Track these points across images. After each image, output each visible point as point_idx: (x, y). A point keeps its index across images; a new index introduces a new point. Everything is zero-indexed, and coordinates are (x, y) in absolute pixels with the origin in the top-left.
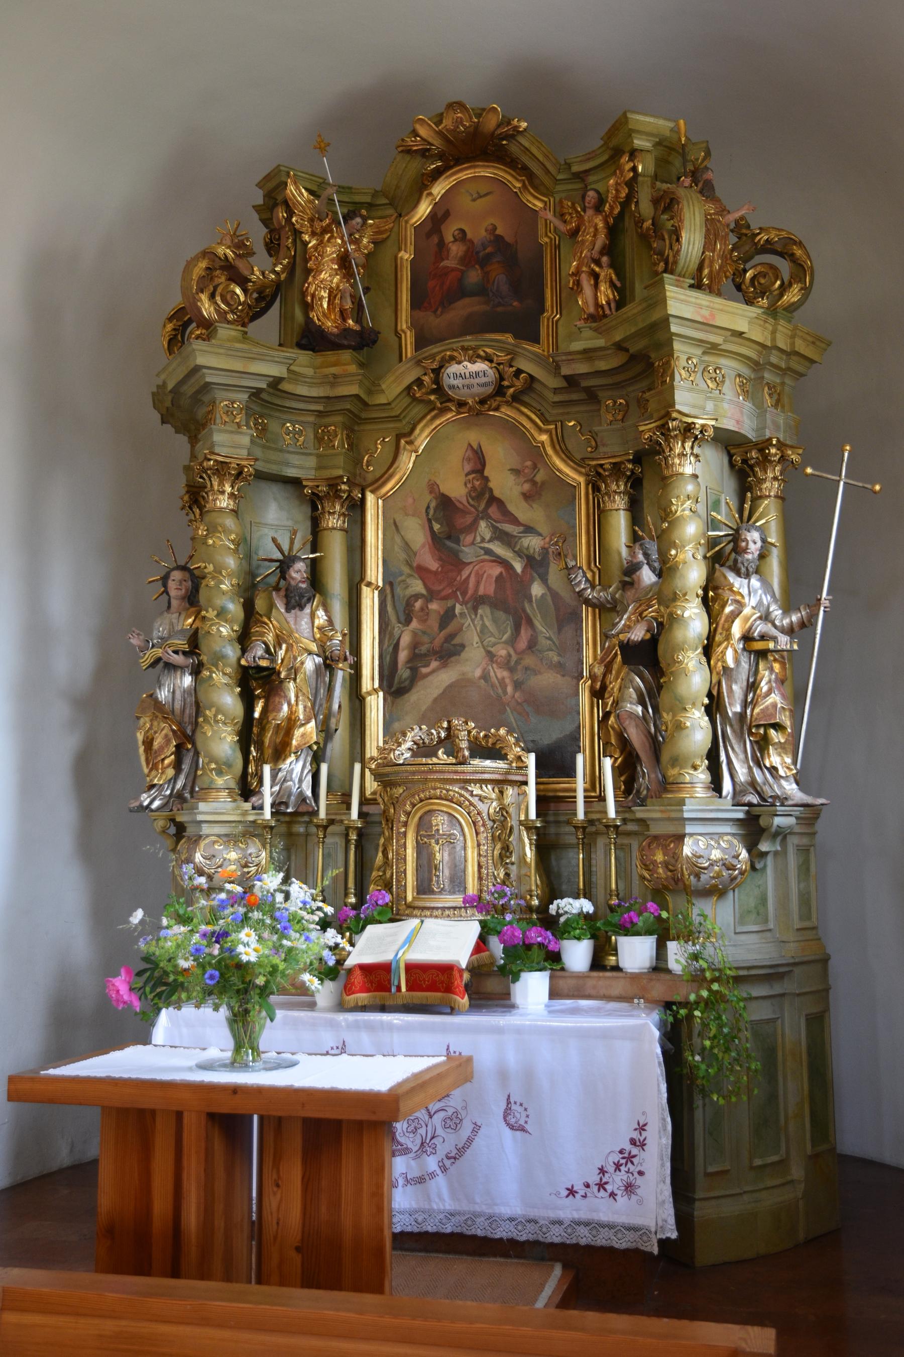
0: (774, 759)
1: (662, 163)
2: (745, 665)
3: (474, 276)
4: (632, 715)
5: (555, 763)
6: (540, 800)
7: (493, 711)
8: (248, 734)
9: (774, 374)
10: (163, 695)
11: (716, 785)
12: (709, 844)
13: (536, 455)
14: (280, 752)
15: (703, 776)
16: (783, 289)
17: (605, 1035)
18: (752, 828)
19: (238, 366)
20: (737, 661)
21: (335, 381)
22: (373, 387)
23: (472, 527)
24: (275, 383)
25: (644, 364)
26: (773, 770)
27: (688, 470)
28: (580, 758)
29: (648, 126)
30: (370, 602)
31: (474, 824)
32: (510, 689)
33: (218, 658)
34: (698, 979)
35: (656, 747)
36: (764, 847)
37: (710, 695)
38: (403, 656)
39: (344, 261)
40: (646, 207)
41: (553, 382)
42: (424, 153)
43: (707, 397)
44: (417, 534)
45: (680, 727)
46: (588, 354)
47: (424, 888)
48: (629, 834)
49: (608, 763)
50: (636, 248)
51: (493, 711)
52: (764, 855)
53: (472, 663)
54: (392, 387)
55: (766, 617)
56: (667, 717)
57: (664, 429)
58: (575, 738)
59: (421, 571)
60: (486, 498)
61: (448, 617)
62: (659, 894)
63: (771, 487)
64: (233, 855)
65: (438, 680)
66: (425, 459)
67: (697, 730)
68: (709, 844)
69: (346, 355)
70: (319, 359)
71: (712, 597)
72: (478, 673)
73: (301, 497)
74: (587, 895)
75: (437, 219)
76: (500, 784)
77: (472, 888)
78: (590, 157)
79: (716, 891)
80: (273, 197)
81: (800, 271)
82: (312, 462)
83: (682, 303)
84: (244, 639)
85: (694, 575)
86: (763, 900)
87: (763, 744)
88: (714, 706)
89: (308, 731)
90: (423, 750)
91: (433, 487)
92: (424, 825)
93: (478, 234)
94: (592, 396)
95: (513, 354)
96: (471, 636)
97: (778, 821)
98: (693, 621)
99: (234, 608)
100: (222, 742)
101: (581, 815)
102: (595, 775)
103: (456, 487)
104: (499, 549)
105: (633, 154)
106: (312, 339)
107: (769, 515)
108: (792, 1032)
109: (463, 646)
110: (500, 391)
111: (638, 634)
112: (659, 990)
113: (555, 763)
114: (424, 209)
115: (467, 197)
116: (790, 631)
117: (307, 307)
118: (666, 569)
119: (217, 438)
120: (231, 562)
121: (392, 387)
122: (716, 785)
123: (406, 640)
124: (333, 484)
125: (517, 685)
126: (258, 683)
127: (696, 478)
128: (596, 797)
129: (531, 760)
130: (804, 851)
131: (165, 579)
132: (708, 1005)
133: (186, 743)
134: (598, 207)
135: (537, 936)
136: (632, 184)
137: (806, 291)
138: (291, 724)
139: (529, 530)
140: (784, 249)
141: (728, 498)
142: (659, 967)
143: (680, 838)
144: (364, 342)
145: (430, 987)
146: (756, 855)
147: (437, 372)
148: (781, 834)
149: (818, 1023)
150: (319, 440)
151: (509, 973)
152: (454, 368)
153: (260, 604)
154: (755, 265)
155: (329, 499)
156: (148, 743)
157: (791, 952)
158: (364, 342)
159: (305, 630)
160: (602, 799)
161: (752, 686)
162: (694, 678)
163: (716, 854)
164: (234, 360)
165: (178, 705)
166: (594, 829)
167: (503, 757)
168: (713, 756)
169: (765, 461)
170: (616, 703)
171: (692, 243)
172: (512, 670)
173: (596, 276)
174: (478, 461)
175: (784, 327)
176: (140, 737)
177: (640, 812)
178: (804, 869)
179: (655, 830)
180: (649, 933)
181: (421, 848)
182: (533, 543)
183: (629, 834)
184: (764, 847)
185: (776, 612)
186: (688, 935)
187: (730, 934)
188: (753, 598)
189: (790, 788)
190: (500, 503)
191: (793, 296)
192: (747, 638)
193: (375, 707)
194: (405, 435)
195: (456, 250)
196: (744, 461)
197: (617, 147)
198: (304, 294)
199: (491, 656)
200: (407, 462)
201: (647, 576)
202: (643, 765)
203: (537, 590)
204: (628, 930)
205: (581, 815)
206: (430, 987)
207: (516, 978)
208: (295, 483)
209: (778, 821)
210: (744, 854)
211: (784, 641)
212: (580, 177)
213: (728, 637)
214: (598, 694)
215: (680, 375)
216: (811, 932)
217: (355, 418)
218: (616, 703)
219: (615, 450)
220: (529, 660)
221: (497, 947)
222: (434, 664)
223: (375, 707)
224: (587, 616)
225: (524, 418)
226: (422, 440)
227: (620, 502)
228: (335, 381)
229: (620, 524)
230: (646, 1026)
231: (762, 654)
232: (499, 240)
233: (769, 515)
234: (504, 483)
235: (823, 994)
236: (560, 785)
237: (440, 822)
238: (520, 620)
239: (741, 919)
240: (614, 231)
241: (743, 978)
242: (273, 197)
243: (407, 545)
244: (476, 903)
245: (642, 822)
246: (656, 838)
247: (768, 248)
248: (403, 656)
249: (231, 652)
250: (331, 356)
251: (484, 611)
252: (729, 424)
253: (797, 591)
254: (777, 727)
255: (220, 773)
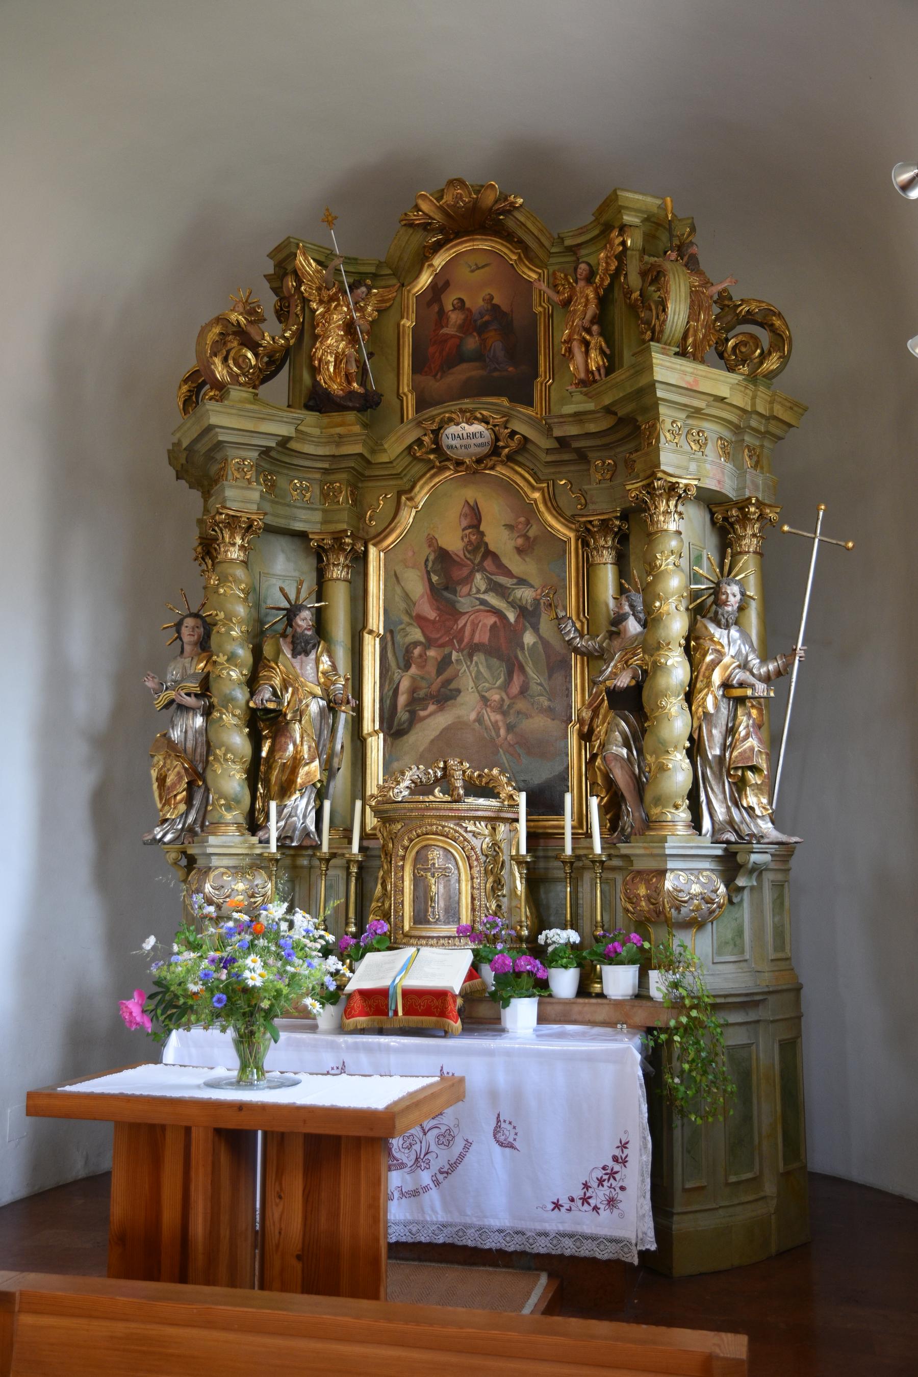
0: (751, 799)
1: (650, 237)
2: (724, 711)
3: (472, 343)
4: (618, 757)
5: (544, 802)
6: (531, 836)
7: (487, 752)
8: (255, 773)
9: (754, 437)
10: (176, 735)
11: (696, 824)
12: (689, 879)
13: (529, 512)
14: (286, 789)
15: (684, 815)
16: (763, 357)
17: (590, 1058)
18: (730, 864)
19: (249, 425)
20: (717, 707)
21: (340, 440)
22: (376, 446)
23: (469, 579)
24: (284, 442)
25: (631, 427)
26: (750, 809)
27: (672, 527)
28: (568, 797)
29: (637, 203)
30: (371, 649)
31: (469, 857)
32: (502, 732)
33: (228, 700)
34: (678, 1006)
35: (640, 788)
36: (741, 882)
37: (691, 739)
38: (402, 699)
39: (349, 328)
40: (634, 279)
41: (545, 443)
42: (426, 227)
43: (690, 458)
44: (415, 584)
45: (662, 768)
46: (578, 417)
47: (420, 918)
48: (613, 869)
49: (594, 802)
50: (624, 318)
51: (487, 752)
52: (741, 889)
53: (467, 707)
54: (394, 447)
55: (744, 666)
56: (650, 759)
57: (649, 488)
58: (563, 778)
59: (420, 620)
60: (481, 551)
61: (444, 663)
62: (642, 925)
63: (750, 543)
64: (241, 886)
65: (435, 723)
66: (426, 513)
67: (679, 771)
68: (689, 879)
69: (351, 416)
70: (325, 420)
71: (693, 646)
72: (473, 716)
73: (308, 549)
74: (574, 926)
75: (438, 289)
76: (493, 821)
77: (465, 918)
78: (582, 231)
79: (696, 924)
80: (283, 267)
81: (779, 340)
82: (318, 516)
83: (667, 369)
84: (252, 683)
85: (677, 625)
86: (740, 933)
87: (740, 785)
88: (695, 749)
89: (312, 770)
90: (421, 788)
91: (431, 541)
92: (421, 859)
93: (476, 303)
94: (582, 457)
95: (508, 417)
96: (467, 682)
97: (754, 858)
98: (676, 669)
99: (244, 653)
100: (231, 779)
101: (568, 851)
102: (582, 815)
103: (453, 542)
104: (493, 600)
105: (623, 229)
106: (319, 401)
107: (748, 570)
108: (766, 1056)
109: (459, 691)
110: (495, 451)
111: (624, 681)
112: (641, 1016)
113: (544, 802)
114: (425, 279)
115: (466, 269)
116: (767, 679)
117: (315, 371)
118: (650, 620)
119: (229, 493)
120: (241, 610)
121: (394, 447)
122: (696, 824)
123: (405, 684)
124: (338, 538)
125: (510, 728)
126: (265, 724)
127: (680, 533)
128: (582, 834)
129: (522, 798)
130: (779, 887)
131: (178, 626)
132: (687, 1030)
133: (198, 780)
134: (589, 279)
135: (526, 964)
136: (621, 257)
137: (785, 360)
138: (296, 763)
139: (522, 582)
140: (764, 319)
141: (710, 553)
142: (641, 994)
143: (662, 873)
144: (367, 404)
145: (425, 1012)
146: (733, 889)
147: (436, 433)
148: (757, 870)
149: (790, 1049)
150: (325, 496)
151: (500, 999)
152: (452, 430)
153: (268, 650)
154: (738, 334)
155: (334, 551)
156: (162, 780)
157: (766, 981)
158: (367, 404)
159: (308, 678)
160: (589, 836)
161: (731, 731)
162: (676, 722)
163: (696, 889)
164: (245, 420)
165: (190, 744)
166: (580, 864)
167: (496, 796)
168: (693, 796)
169: (745, 519)
170: (603, 746)
171: (677, 313)
172: (505, 714)
173: (587, 344)
174: (474, 516)
175: (763, 393)
176: (154, 774)
177: (624, 848)
178: (779, 903)
179: (639, 865)
180: (632, 962)
181: (419, 882)
182: (526, 595)
183: (613, 869)
184: (741, 882)
185: (755, 662)
186: (669, 965)
187: (708, 964)
188: (732, 646)
189: (766, 826)
190: (495, 556)
191: (772, 364)
192: (726, 685)
193: (376, 747)
194: (406, 492)
195: (455, 318)
196: (725, 519)
197: (608, 223)
198: (311, 358)
199: (485, 700)
200: (408, 517)
201: (633, 626)
202: (628, 804)
203: (529, 638)
204: (612, 959)
205: (568, 851)
206: (425, 1012)
207: (506, 1004)
208: (302, 536)
209: (754, 858)
210: (722, 889)
211: (761, 689)
212: (572, 250)
213: (709, 684)
214: (586, 736)
215: (665, 437)
216: (784, 962)
217: (360, 474)
218: (603, 746)
219: (603, 506)
220: (521, 705)
221: (488, 974)
222: (432, 708)
223: (376, 747)
224: (576, 662)
225: (518, 476)
226: (422, 496)
227: (608, 557)
228: (340, 440)
229: (607, 577)
230: (628, 1050)
231: (741, 701)
232: (496, 308)
233: (748, 570)
234: (499, 538)
235: (796, 1021)
236: (550, 822)
237: (436, 857)
238: (513, 667)
239: (719, 951)
240: (604, 301)
241: (720, 1005)
242: (283, 267)
243: (407, 596)
244: (469, 933)
245: (626, 858)
246: (639, 872)
247: (749, 318)
248: (402, 699)
249: (241, 695)
250: (336, 417)
251: (479, 658)
252: (710, 484)
253: (775, 641)
254: (755, 769)
255: (229, 808)
